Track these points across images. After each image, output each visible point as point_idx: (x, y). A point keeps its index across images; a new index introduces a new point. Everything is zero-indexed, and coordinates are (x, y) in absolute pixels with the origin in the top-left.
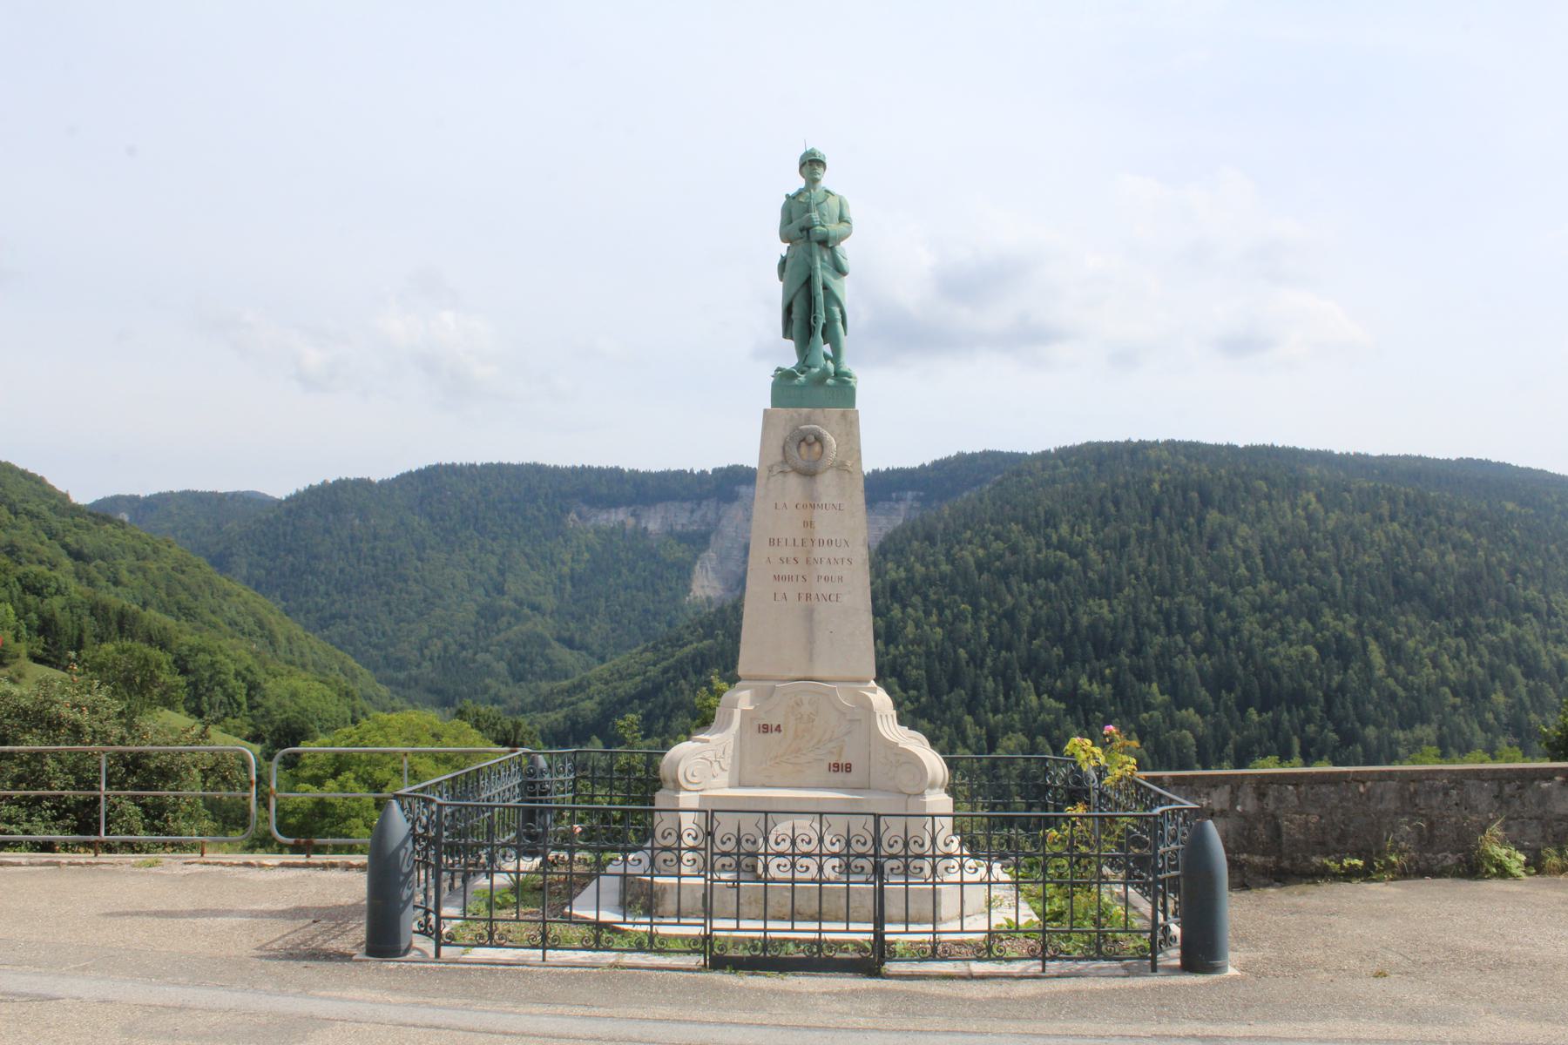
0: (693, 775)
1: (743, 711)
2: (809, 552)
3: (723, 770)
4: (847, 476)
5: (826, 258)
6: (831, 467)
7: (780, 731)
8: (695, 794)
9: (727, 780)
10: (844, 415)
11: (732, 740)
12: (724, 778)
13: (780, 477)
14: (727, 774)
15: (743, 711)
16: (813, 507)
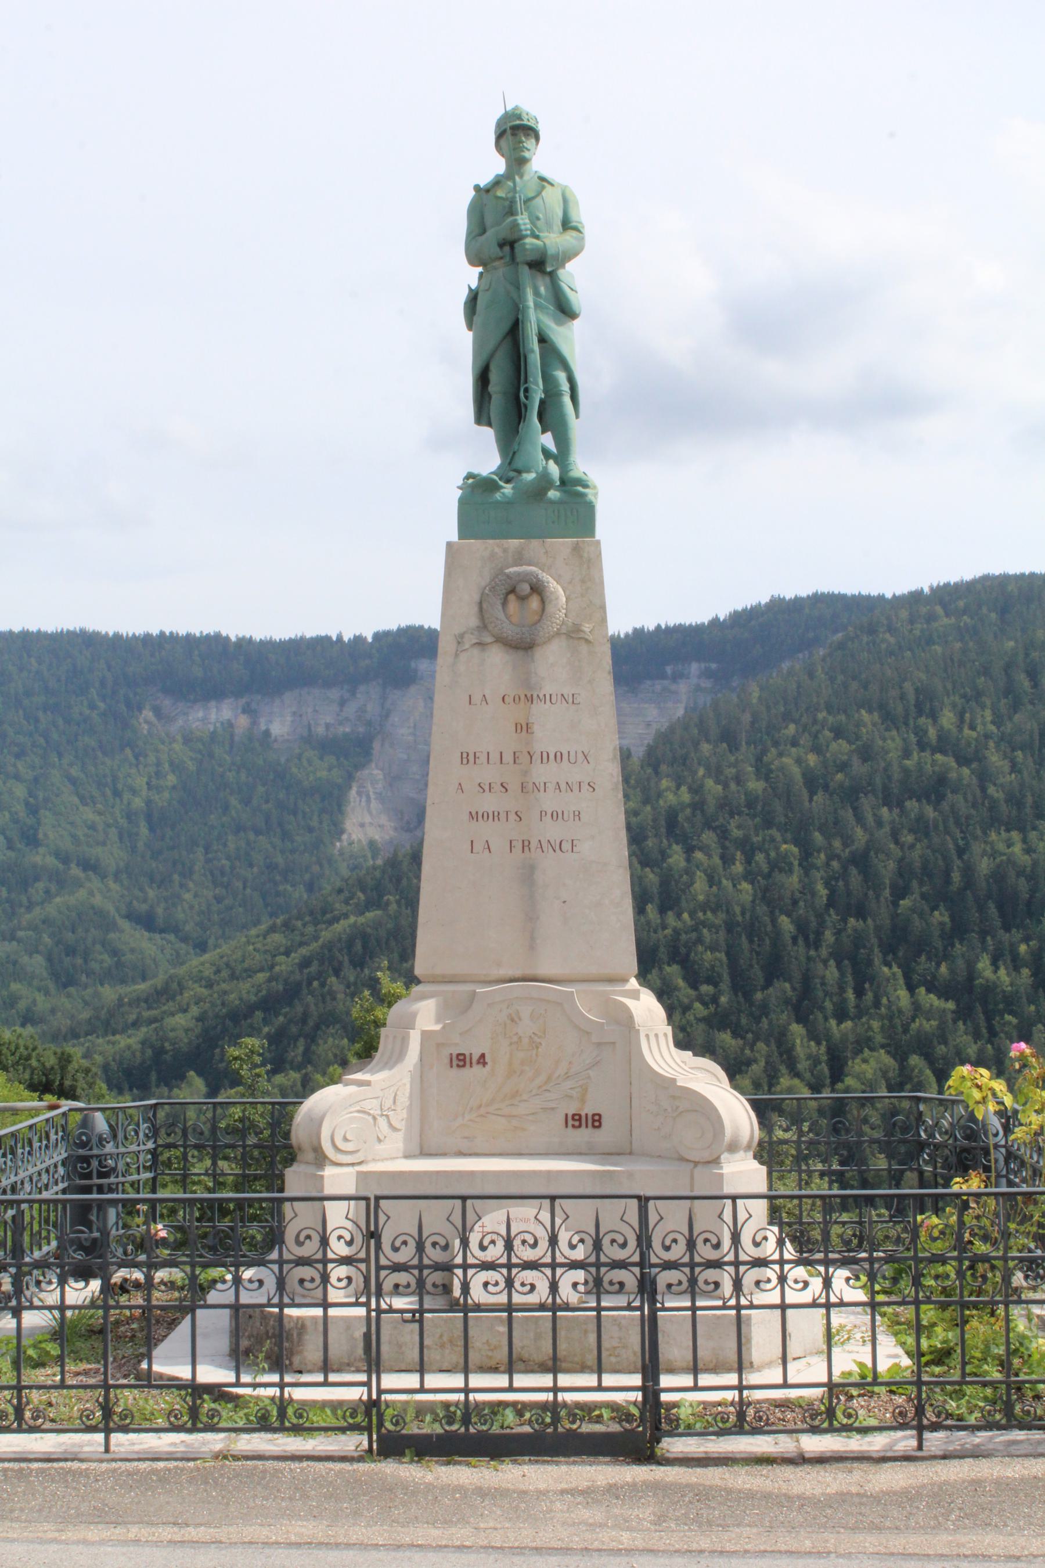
0: (345, 1139)
1: (424, 1033)
2: (526, 773)
3: (395, 1129)
4: (584, 648)
5: (542, 290)
6: (558, 634)
7: (485, 1064)
8: (350, 1169)
9: (401, 1145)
10: (576, 549)
11: (407, 1080)
12: (396, 1143)
13: (475, 651)
14: (400, 1136)
15: (424, 1033)
16: (530, 699)
